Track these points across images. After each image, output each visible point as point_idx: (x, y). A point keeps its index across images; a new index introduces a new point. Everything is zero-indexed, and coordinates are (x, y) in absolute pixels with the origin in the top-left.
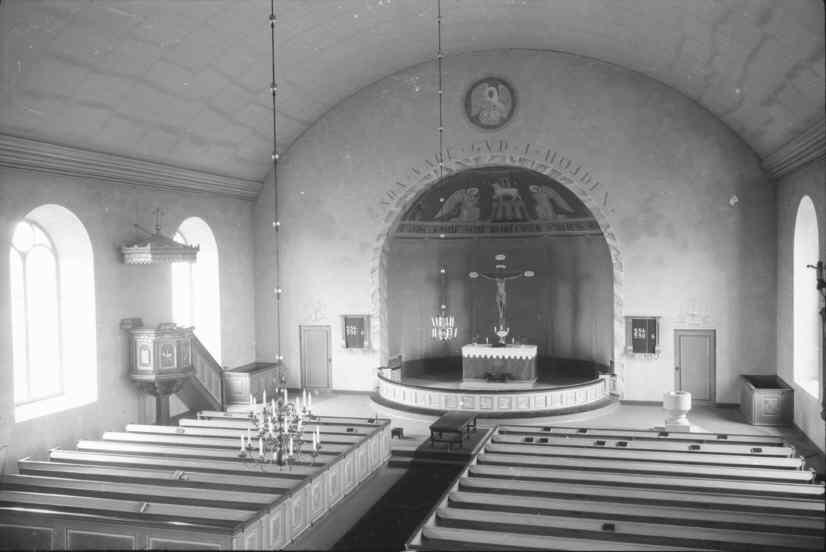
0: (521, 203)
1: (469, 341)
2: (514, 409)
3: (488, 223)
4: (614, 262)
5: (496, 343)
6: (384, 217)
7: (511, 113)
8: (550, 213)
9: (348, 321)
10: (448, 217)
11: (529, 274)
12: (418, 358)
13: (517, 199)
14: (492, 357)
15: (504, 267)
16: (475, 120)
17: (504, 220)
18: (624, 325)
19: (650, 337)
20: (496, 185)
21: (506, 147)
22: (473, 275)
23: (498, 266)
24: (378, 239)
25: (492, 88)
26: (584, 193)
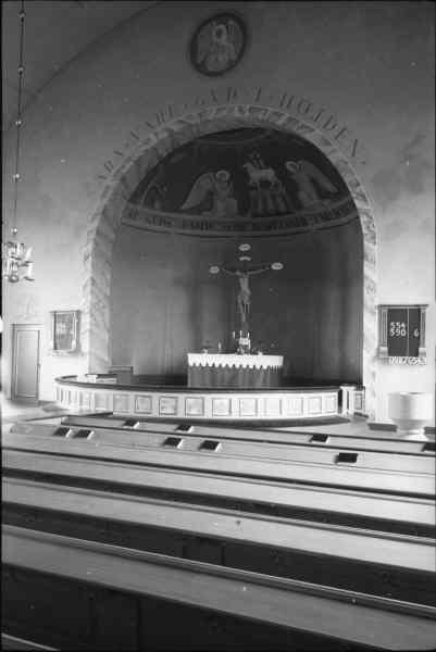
0: (282, 190)
1: (198, 350)
3: (248, 218)
4: (365, 231)
6: (101, 192)
7: (241, 55)
8: (316, 201)
9: (56, 317)
10: (197, 210)
12: (159, 373)
13: (276, 186)
14: (220, 366)
15: (248, 259)
16: (200, 68)
17: (266, 214)
19: (412, 332)
20: (248, 165)
21: (235, 94)
23: (242, 259)
24: (93, 219)
25: (222, 27)
26: (328, 144)
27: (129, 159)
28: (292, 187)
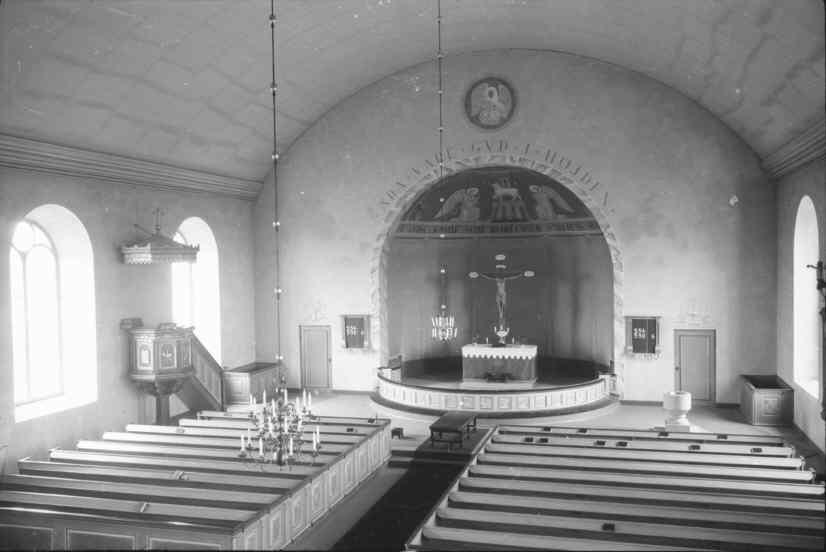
0: (521, 203)
1: (469, 341)
2: (514, 409)
3: (488, 223)
4: (614, 262)
5: (496, 343)
6: (384, 217)
7: (511, 113)
8: (550, 213)
9: (348, 321)
10: (448, 217)
11: (529, 274)
12: (418, 358)
13: (517, 199)
14: (492, 357)
15: (504, 267)
16: (475, 120)
17: (504, 220)
18: (624, 325)
20: (496, 185)
21: (506, 147)
22: (473, 275)
23: (498, 266)
24: (378, 239)
25: (492, 88)
26: (584, 193)
27: (411, 190)
28: (530, 202)
